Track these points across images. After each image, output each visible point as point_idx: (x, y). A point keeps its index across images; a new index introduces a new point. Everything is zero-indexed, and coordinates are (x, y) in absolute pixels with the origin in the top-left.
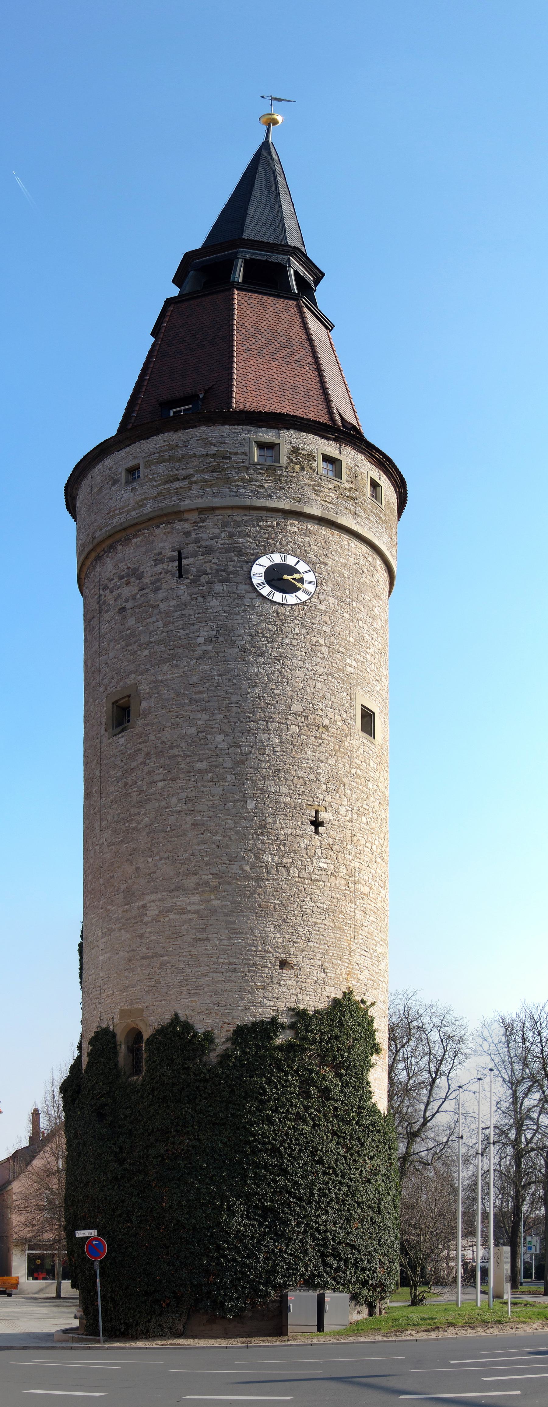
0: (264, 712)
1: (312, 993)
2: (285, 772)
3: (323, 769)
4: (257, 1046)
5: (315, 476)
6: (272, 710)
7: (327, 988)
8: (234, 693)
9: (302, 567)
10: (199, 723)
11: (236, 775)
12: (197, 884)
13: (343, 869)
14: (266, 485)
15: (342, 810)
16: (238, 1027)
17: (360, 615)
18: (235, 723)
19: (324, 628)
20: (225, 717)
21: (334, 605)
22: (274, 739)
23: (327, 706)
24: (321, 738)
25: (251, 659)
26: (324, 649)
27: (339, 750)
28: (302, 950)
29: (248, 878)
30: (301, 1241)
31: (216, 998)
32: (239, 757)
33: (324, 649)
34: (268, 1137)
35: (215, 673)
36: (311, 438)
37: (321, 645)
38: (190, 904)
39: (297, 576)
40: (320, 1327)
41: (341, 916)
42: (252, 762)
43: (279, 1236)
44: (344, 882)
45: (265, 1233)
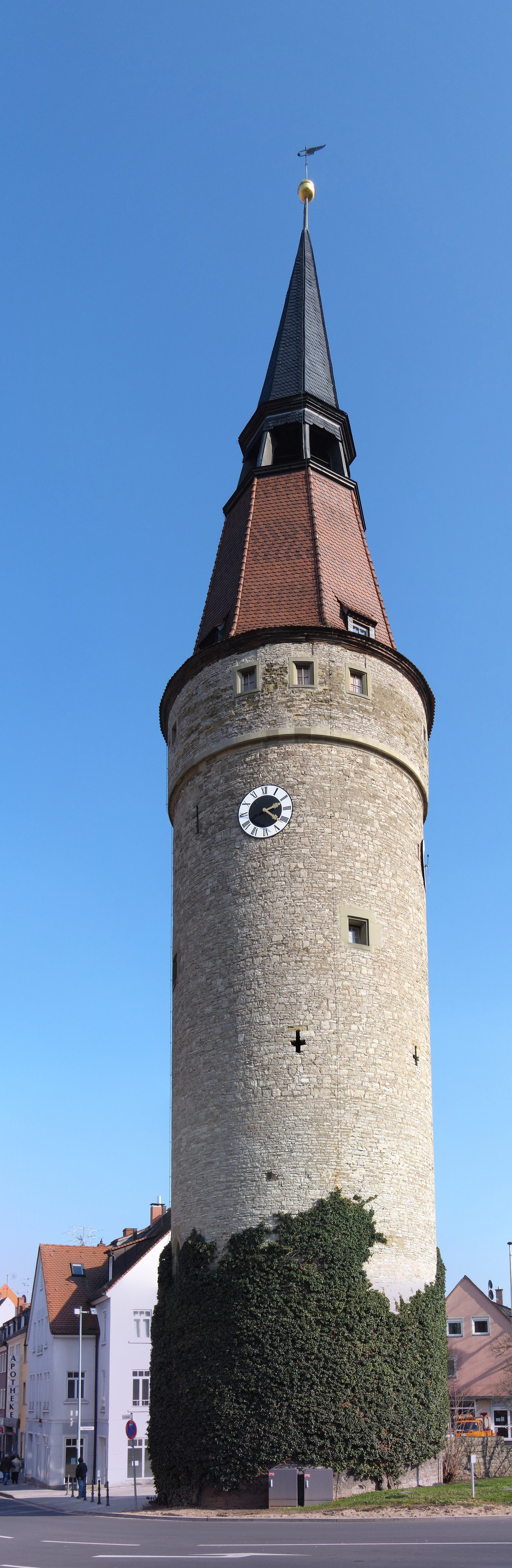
0: (250, 949)
1: (296, 1197)
2: (269, 1001)
3: (304, 990)
4: (245, 1251)
5: (288, 691)
6: (256, 946)
7: (312, 1192)
8: (229, 937)
9: (280, 794)
10: (208, 970)
11: (230, 1013)
12: (206, 1116)
13: (327, 1080)
14: (247, 717)
15: (325, 1025)
16: (233, 1235)
17: (345, 825)
18: (229, 965)
19: (303, 851)
20: (224, 961)
21: (313, 823)
22: (259, 973)
23: (307, 928)
24: (301, 961)
25: (241, 901)
26: (304, 873)
27: (321, 968)
28: (285, 1161)
29: (240, 1104)
30: (283, 1422)
31: (218, 1213)
32: (233, 996)
33: (304, 873)
34: (252, 1331)
35: (217, 921)
36: (282, 648)
37: (300, 869)
38: (203, 1134)
39: (275, 806)
40: (301, 1502)
41: (325, 1124)
42: (242, 999)
43: (262, 1418)
44: (329, 1091)
45: (252, 1416)
